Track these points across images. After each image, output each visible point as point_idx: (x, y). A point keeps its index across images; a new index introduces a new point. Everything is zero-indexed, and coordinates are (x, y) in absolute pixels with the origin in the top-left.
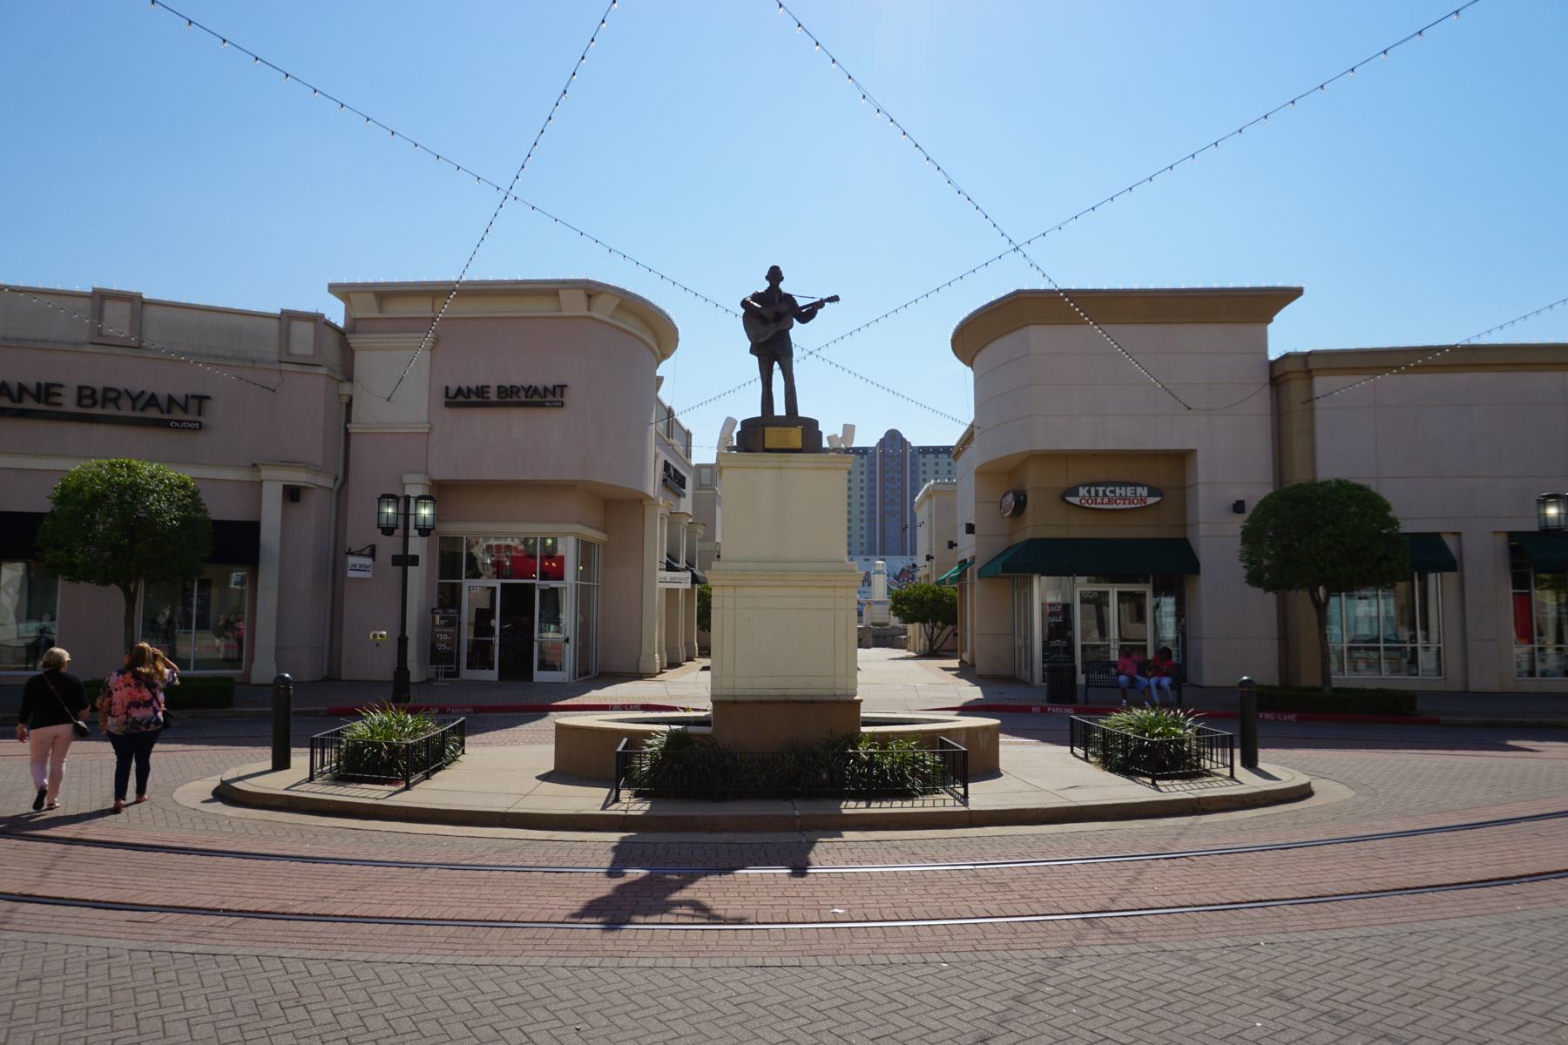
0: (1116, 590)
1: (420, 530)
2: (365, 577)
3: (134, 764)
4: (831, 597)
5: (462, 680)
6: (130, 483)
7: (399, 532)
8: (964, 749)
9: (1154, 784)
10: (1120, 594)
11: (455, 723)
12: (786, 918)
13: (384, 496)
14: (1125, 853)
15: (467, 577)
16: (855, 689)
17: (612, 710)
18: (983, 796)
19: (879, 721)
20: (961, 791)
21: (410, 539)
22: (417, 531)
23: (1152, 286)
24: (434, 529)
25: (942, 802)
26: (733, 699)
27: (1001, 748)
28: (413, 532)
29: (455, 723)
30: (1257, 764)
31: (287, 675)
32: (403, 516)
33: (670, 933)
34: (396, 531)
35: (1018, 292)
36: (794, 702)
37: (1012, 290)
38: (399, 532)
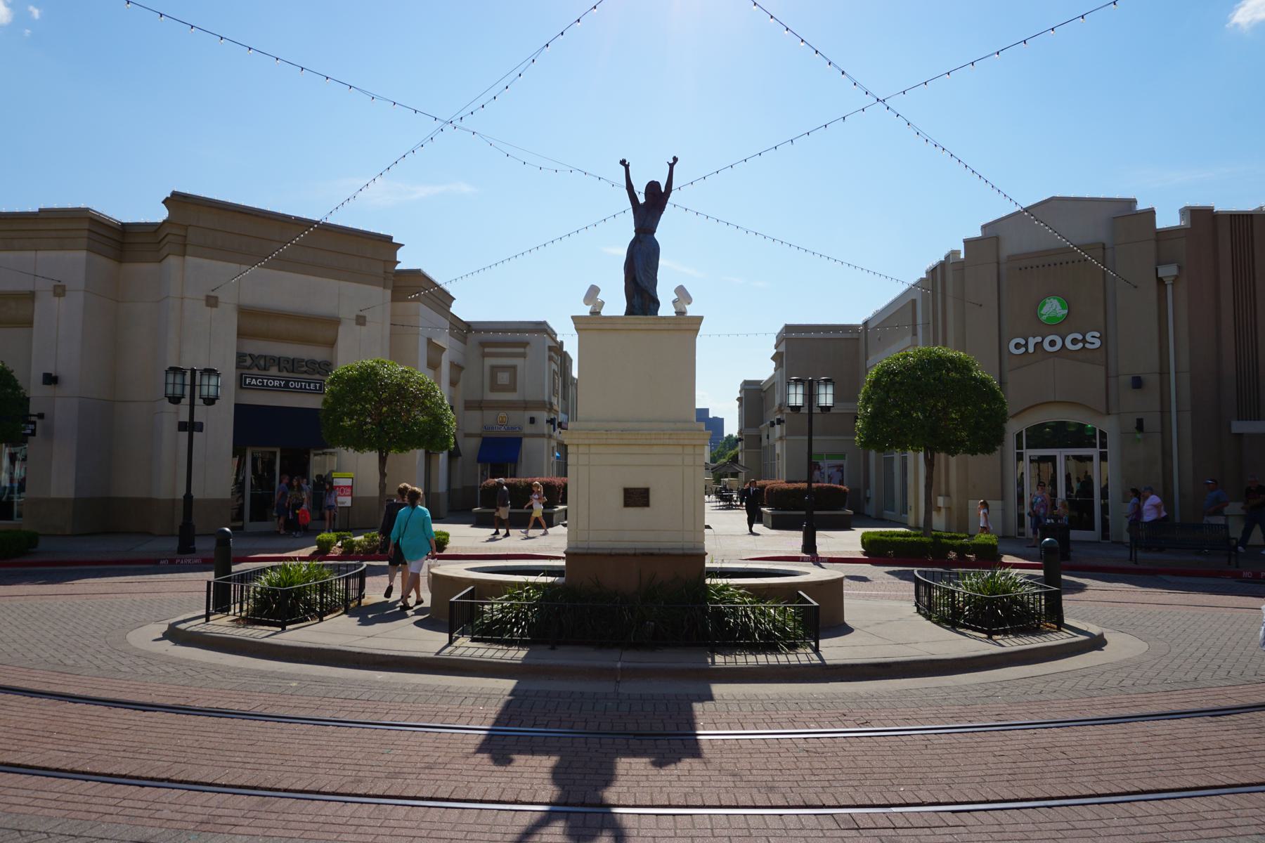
0: (1063, 455)
1: (204, 399)
2: (1174, 454)
3: (427, 616)
4: (587, 454)
5: (1027, 539)
6: (877, 373)
7: (186, 401)
8: (816, 604)
9: (990, 637)
10: (1067, 458)
11: (357, 571)
12: (715, 797)
13: (171, 369)
14: (1055, 718)
15: (1027, 448)
16: (703, 543)
17: (802, 561)
18: (833, 650)
19: (784, 573)
20: (813, 644)
21: (196, 407)
22: (202, 400)
23: (269, 209)
24: (217, 399)
25: (803, 657)
26: (681, 552)
27: (1064, 604)
28: (198, 401)
29: (357, 571)
30: (1063, 621)
31: (227, 529)
32: (189, 387)
33: (461, 814)
34: (183, 400)
35: (87, 210)
36: (596, 554)
37: (83, 205)
38: (186, 401)
